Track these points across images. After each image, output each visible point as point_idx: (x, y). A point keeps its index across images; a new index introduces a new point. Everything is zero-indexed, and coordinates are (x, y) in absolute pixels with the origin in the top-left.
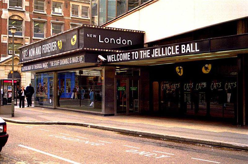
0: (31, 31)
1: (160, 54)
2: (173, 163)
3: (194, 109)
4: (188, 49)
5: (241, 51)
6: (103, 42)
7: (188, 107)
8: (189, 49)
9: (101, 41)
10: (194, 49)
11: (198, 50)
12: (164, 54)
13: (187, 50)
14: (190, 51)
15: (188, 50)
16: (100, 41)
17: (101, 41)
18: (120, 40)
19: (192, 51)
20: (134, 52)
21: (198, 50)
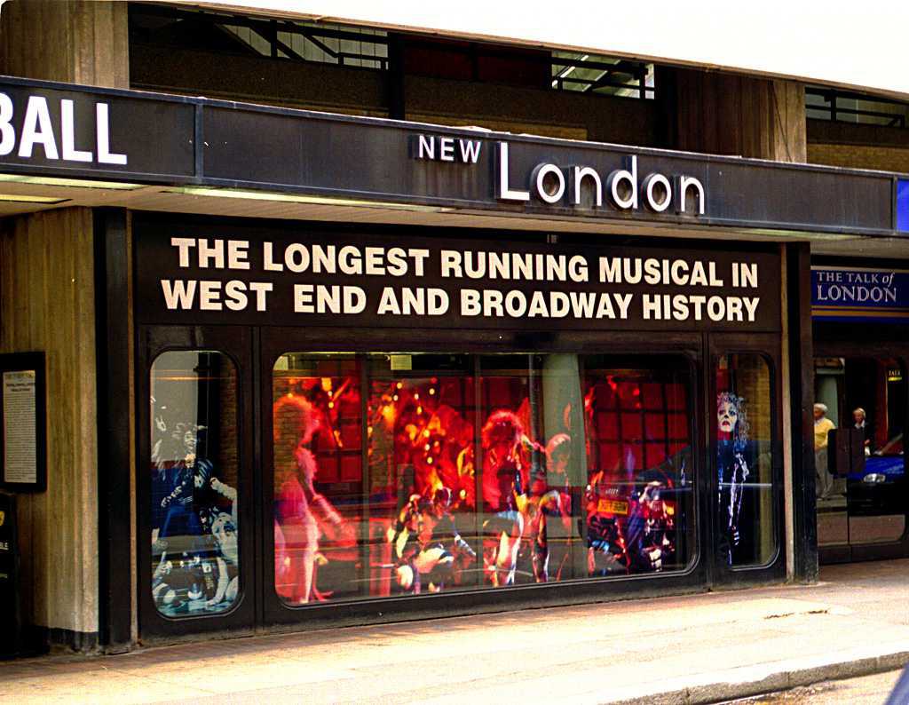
0: (710, 162)
1: (275, 261)
2: (666, 702)
3: (659, 563)
4: (38, 130)
5: (456, 125)
6: (524, 196)
7: (819, 544)
8: (47, 138)
9: (511, 187)
10: (86, 139)
11: (121, 159)
12: (717, 278)
13: (29, 137)
14: (51, 153)
15: (38, 138)
16: (506, 194)
17: (511, 187)
18: (633, 180)
19: (70, 154)
20: (703, 299)
21: (121, 159)
